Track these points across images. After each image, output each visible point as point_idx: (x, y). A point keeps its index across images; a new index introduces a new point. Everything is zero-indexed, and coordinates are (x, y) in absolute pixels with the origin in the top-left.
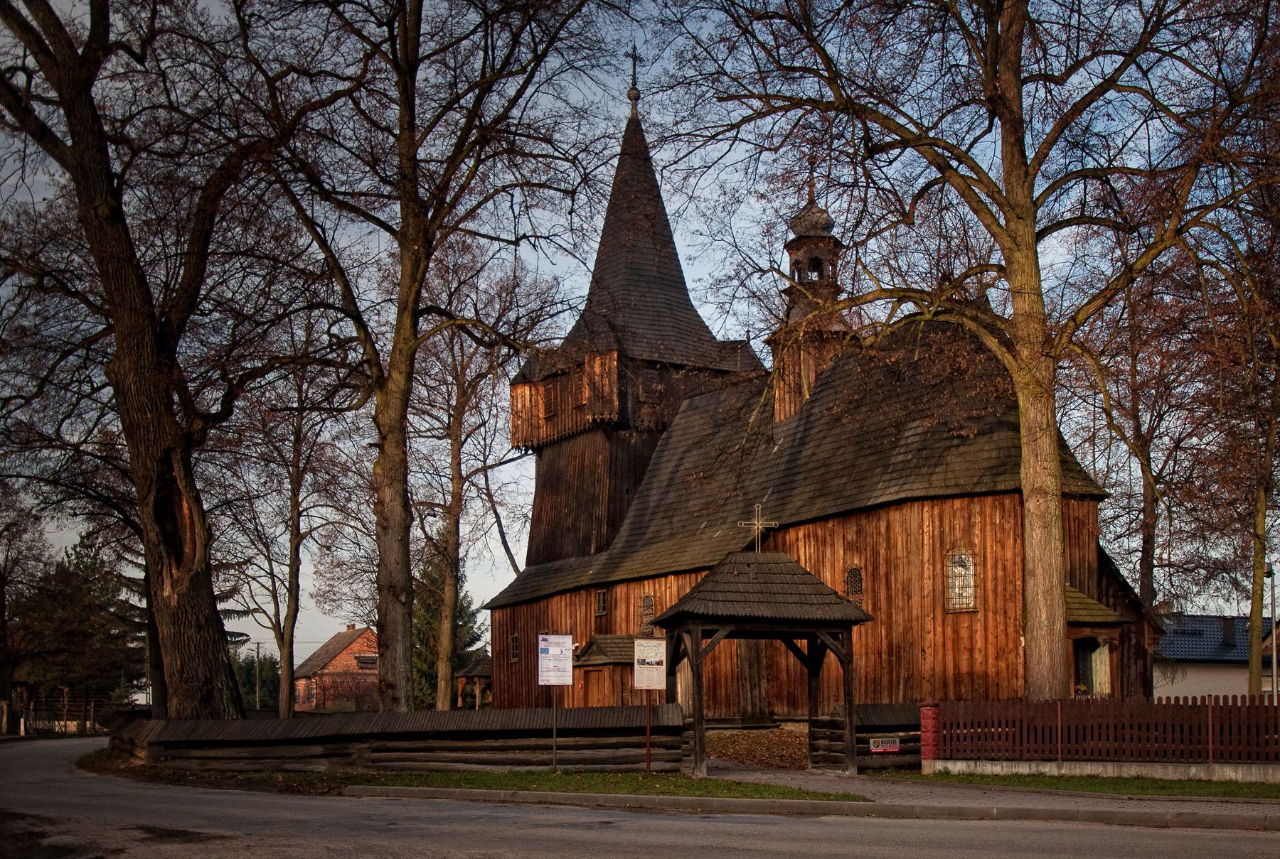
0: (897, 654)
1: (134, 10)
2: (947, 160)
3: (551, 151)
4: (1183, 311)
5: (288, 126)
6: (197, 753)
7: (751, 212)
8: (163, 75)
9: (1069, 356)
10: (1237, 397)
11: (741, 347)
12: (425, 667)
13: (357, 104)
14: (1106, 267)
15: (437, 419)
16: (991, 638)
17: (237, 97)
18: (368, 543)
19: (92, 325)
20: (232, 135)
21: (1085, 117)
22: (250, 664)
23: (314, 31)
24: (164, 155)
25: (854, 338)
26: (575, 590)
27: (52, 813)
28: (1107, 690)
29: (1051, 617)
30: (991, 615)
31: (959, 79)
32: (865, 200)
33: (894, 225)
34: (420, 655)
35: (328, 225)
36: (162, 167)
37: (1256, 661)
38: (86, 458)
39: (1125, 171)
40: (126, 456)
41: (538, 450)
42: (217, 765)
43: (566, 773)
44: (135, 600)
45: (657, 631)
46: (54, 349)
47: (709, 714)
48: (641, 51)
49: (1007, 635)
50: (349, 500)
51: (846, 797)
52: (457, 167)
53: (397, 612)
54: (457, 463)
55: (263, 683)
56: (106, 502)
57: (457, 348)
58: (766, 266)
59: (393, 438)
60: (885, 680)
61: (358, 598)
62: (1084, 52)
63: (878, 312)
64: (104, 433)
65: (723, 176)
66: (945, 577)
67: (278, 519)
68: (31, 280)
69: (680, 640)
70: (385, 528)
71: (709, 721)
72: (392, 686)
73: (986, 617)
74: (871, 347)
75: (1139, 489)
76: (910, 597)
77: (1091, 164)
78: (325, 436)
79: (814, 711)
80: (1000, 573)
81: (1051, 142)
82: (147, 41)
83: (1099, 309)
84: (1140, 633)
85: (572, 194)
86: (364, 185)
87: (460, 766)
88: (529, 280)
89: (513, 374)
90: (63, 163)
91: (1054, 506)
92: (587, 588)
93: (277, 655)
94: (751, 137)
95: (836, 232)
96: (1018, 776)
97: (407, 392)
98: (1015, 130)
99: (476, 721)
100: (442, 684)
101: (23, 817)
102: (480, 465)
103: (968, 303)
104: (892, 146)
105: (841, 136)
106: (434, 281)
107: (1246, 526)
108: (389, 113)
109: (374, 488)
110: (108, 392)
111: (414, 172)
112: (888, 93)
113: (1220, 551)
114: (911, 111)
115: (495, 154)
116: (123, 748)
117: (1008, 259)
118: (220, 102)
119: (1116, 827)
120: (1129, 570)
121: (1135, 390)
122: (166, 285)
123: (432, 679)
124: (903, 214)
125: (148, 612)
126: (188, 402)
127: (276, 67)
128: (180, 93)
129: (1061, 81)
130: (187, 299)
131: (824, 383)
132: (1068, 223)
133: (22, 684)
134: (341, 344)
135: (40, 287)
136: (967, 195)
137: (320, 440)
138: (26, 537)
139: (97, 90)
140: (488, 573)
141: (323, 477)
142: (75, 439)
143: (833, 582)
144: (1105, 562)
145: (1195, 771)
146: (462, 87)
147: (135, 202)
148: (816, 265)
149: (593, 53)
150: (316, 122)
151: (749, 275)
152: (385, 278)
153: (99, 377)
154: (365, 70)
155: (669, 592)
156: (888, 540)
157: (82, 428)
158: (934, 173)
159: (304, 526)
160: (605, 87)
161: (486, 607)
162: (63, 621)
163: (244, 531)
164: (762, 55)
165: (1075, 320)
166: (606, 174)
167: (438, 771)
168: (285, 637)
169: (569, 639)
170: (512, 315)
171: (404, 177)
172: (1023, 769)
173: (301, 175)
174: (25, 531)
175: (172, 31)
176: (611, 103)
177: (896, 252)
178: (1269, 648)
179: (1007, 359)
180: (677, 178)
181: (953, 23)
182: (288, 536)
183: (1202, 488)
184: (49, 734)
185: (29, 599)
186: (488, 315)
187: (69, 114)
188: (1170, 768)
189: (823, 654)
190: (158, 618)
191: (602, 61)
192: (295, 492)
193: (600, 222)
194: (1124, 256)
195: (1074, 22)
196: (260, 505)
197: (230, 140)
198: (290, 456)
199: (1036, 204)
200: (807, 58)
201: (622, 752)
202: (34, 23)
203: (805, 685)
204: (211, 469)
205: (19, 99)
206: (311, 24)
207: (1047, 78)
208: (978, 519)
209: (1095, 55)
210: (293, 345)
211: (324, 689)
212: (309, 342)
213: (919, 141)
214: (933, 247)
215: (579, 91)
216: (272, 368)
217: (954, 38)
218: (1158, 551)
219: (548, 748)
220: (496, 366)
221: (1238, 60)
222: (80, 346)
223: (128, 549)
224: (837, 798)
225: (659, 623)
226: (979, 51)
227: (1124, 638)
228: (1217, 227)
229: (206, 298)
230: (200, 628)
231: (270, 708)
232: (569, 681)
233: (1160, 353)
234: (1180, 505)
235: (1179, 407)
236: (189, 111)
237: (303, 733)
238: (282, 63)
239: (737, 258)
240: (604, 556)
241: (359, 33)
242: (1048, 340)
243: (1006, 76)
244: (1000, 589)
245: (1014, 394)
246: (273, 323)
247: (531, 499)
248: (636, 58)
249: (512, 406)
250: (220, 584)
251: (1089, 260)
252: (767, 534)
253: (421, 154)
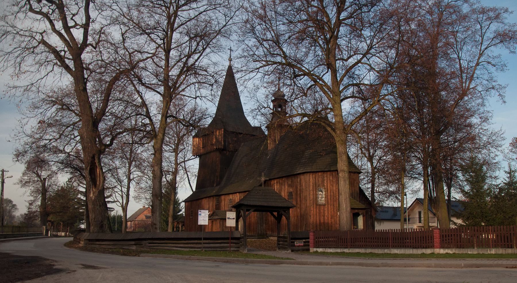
0: (303, 217)
1: (94, 35)
2: (316, 79)
3: (206, 74)
4: (380, 122)
5: (134, 66)
6: (98, 243)
7: (262, 92)
8: (101, 52)
9: (350, 133)
10: (396, 146)
11: (259, 129)
12: (165, 219)
13: (153, 60)
14: (360, 110)
15: (171, 147)
17: (120, 58)
18: (150, 182)
19: (76, 119)
20: (118, 68)
21: (353, 70)
22: (114, 217)
23: (143, 41)
24: (100, 73)
25: (291, 127)
26: (210, 197)
27: (54, 259)
28: (362, 228)
29: (346, 206)
31: (319, 59)
32: (294, 89)
33: (302, 96)
34: (164, 215)
35: (143, 92)
36: (98, 76)
37: (402, 220)
38: (71, 156)
39: (364, 84)
40: (82, 156)
41: (200, 156)
42: (103, 246)
43: (205, 251)
44: (83, 198)
45: (233, 209)
46: (64, 126)
47: (248, 234)
48: (232, 48)
50: (145, 170)
51: (288, 259)
52: (180, 77)
53: (157, 203)
54: (176, 160)
55: (118, 222)
56: (76, 169)
57: (178, 127)
58: (266, 106)
59: (158, 152)
60: (299, 225)
61: (146, 198)
62: (352, 53)
63: (297, 120)
64: (77, 150)
65: (254, 82)
66: (316, 195)
67: (124, 175)
68: (60, 107)
69: (240, 212)
70: (155, 178)
71: (248, 236)
72: (155, 224)
74: (295, 129)
75: (370, 171)
77: (355, 82)
78: (139, 151)
79: (279, 233)
81: (344, 76)
82: (97, 44)
83: (358, 121)
84: (371, 212)
85: (212, 85)
86: (154, 82)
87: (174, 248)
88: (199, 109)
89: (193, 135)
90: (72, 75)
91: (347, 175)
92: (212, 196)
93: (122, 215)
94: (262, 72)
95: (286, 98)
96: (337, 252)
97: (163, 139)
98: (334, 72)
99: (179, 235)
100: (170, 224)
101: (48, 260)
102: (183, 160)
103: (321, 118)
104: (301, 75)
105: (287, 72)
106: (172, 108)
107: (399, 182)
108: (162, 62)
109: (152, 166)
110: (79, 138)
111: (168, 79)
112: (300, 62)
113: (392, 188)
114: (306, 66)
115: (191, 74)
116: (77, 241)
117: (333, 107)
118: (115, 59)
119: (365, 267)
120: (368, 193)
121: (369, 143)
122: (97, 108)
123: (167, 222)
124: (304, 93)
125: (86, 201)
126: (101, 141)
127: (132, 50)
128: (105, 57)
129: (346, 60)
130: (102, 112)
131: (282, 139)
132: (349, 97)
133: (50, 221)
134: (145, 125)
135: (62, 109)
136: (322, 89)
137: (137, 152)
138: (53, 179)
139: (82, 56)
140: (184, 191)
141: (138, 163)
142: (68, 151)
143: (285, 196)
144: (361, 192)
145: (386, 251)
146: (182, 56)
147: (90, 86)
148: (280, 106)
149: (219, 48)
150: (142, 65)
151: (261, 109)
152: (158, 107)
153: (76, 133)
154: (156, 51)
155: (237, 198)
156: (300, 184)
157: (71, 148)
158: (313, 83)
159: (131, 177)
160: (222, 57)
161: (183, 201)
162: (62, 203)
163: (114, 178)
164: (266, 50)
165: (352, 124)
166: (222, 80)
167: (168, 250)
168: (125, 209)
169: (207, 211)
170: (194, 118)
171: (165, 80)
172: (339, 250)
173: (136, 79)
174: (53, 177)
175: (104, 41)
176: (224, 61)
177: (302, 103)
178: (406, 216)
179: (333, 134)
180: (241, 82)
181: (317, 44)
182: (127, 180)
183: (387, 171)
184: (57, 236)
185: (53, 197)
186: (187, 118)
187: (74, 62)
188: (380, 250)
189: (282, 217)
190: (88, 203)
191: (222, 50)
192: (130, 167)
193: (219, 93)
194: (365, 107)
195: (349, 46)
196: (119, 171)
197: (117, 69)
198: (129, 157)
199: (341, 92)
200: (278, 51)
201: (222, 245)
202: (68, 39)
203: (277, 227)
204: (106, 160)
205: (62, 58)
206: (142, 39)
207: (342, 59)
208: (326, 178)
209: (355, 54)
210: (131, 125)
211: (136, 225)
212: (136, 125)
213: (308, 74)
214: (313, 102)
215: (214, 58)
216: (125, 132)
217: (318, 48)
218: (375, 188)
219: (201, 243)
220: (189, 132)
221: (392, 58)
222: (72, 125)
223: (81, 183)
224: (285, 259)
225: (234, 207)
226: (324, 52)
227: (367, 213)
228: (388, 100)
229: (108, 112)
230: (100, 206)
231: (120, 230)
232: (207, 224)
233: (375, 133)
234: (381, 175)
235: (380, 148)
236: (107, 61)
237: (129, 238)
238: (133, 49)
239: (258, 104)
240: (218, 187)
241: (155, 42)
242: (344, 129)
243: (332, 59)
245: (335, 143)
246: (126, 119)
247: (197, 170)
248: (231, 50)
249: (193, 143)
250: (107, 194)
251: (355, 108)
252: (265, 181)
253: (170, 74)
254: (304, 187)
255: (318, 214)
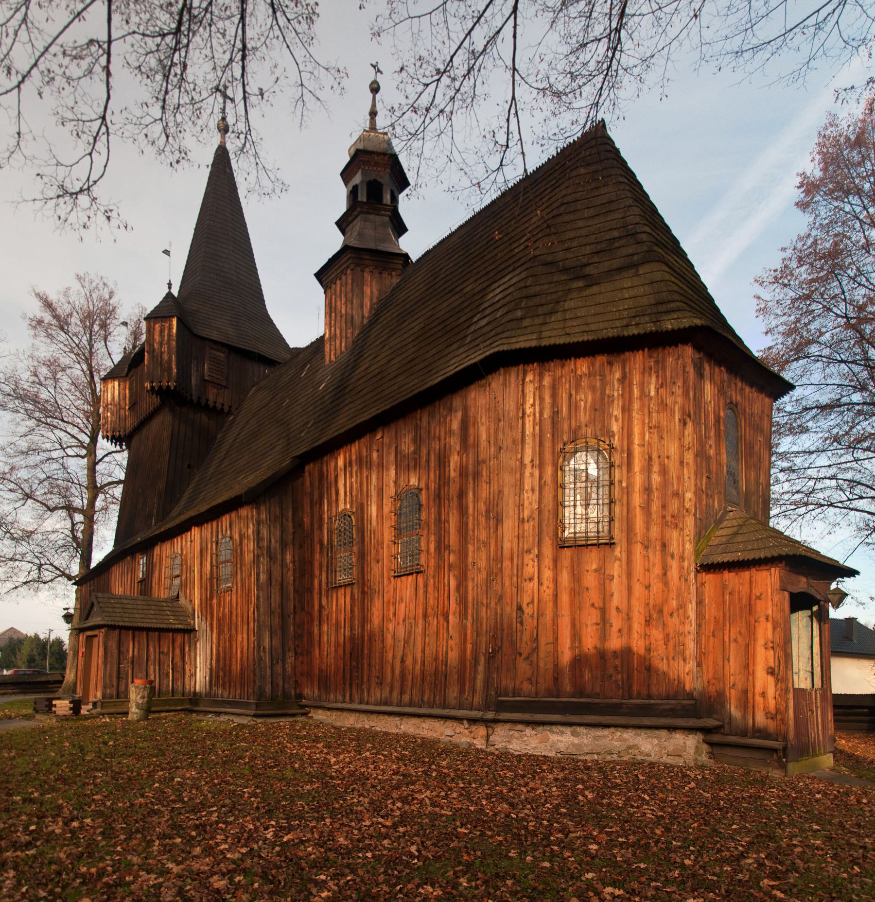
16: (638, 590)
30: (638, 549)
49: (666, 584)
55: (52, 654)
73: (629, 553)
76: (499, 521)
80: (656, 478)
244: (655, 507)
254: (486, 449)
255: (565, 598)
